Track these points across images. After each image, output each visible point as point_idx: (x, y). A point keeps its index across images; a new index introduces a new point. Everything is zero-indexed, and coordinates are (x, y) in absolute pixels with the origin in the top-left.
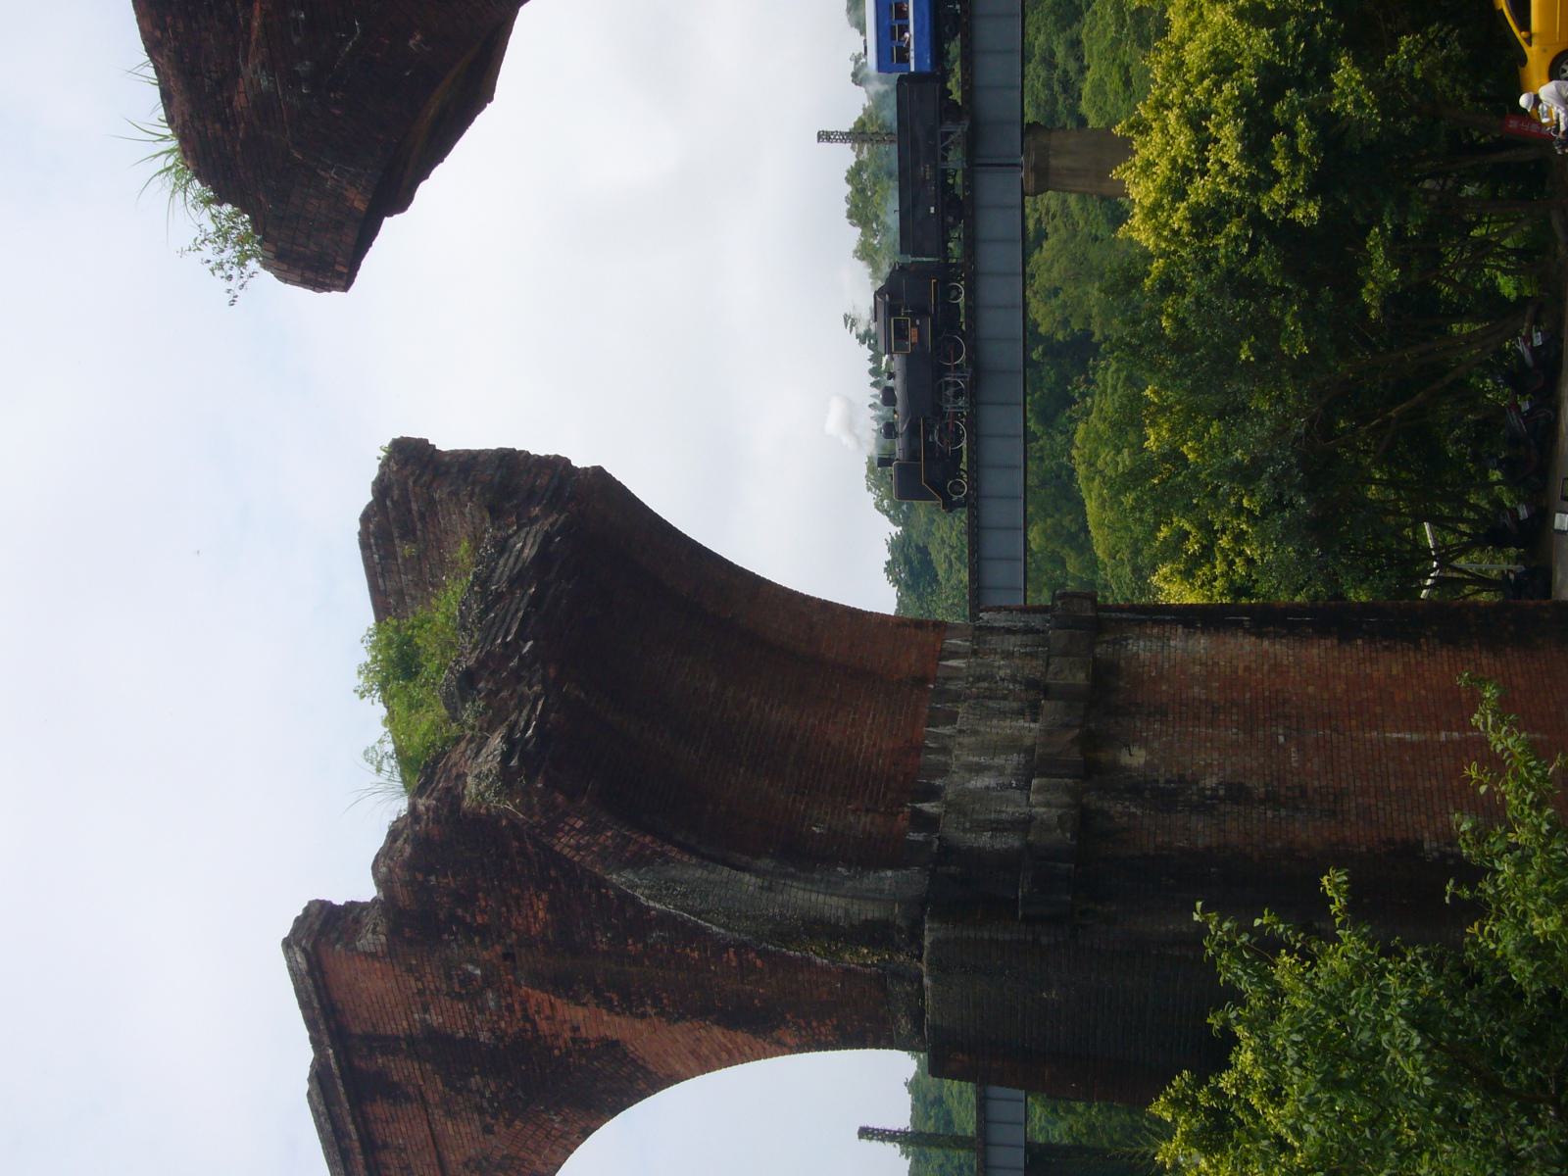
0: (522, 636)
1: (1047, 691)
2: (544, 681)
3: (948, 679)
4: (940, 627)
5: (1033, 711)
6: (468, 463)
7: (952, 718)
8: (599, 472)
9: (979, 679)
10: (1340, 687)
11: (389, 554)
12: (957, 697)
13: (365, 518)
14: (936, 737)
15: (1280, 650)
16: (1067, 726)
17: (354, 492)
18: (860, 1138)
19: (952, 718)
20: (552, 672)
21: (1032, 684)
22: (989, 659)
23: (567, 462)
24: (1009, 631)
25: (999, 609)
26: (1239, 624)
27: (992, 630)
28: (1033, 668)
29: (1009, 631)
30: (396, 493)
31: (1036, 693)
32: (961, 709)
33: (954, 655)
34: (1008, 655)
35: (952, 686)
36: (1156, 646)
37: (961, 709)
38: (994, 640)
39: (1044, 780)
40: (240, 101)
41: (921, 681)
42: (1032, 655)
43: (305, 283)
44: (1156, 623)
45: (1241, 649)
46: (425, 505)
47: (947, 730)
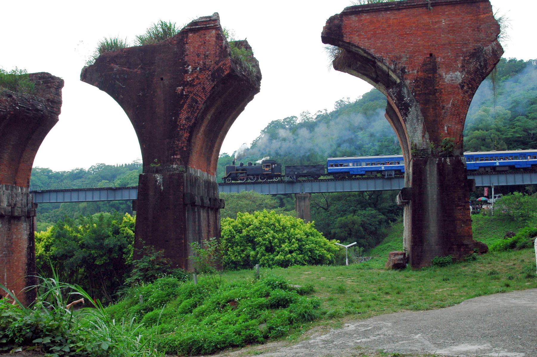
0: (19, 107)
1: (13, 208)
2: (10, 111)
3: (16, 189)
4: (28, 186)
5: (9, 205)
6: (59, 94)
7: (7, 189)
8: (58, 120)
9: (16, 194)
10: (16, 264)
11: (40, 78)
12: (12, 190)
13: (48, 74)
14: (3, 187)
15: (25, 252)
16: (5, 212)
17: (54, 73)
18: (216, 14)
19: (7, 189)
20: (12, 113)
21: (15, 205)
22: (21, 196)
23: (60, 114)
24: (27, 200)
25: (32, 198)
26: (30, 244)
27: (28, 196)
28: (19, 205)
29: (27, 200)
30: (52, 81)
31: (13, 207)
32: (9, 191)
33: (22, 189)
34: (22, 200)
35: (14, 189)
36: (25, 228)
37: (9, 191)
38: (25, 197)
39: (194, 157)
40: (112, 65)
41: (15, 183)
42: (22, 205)
43: (82, 73)
44: (30, 228)
45: (24, 244)
46: (48, 87)
47: (4, 188)
